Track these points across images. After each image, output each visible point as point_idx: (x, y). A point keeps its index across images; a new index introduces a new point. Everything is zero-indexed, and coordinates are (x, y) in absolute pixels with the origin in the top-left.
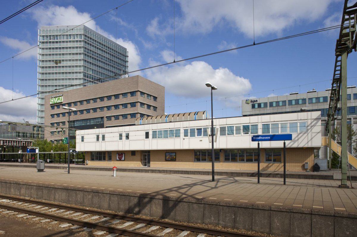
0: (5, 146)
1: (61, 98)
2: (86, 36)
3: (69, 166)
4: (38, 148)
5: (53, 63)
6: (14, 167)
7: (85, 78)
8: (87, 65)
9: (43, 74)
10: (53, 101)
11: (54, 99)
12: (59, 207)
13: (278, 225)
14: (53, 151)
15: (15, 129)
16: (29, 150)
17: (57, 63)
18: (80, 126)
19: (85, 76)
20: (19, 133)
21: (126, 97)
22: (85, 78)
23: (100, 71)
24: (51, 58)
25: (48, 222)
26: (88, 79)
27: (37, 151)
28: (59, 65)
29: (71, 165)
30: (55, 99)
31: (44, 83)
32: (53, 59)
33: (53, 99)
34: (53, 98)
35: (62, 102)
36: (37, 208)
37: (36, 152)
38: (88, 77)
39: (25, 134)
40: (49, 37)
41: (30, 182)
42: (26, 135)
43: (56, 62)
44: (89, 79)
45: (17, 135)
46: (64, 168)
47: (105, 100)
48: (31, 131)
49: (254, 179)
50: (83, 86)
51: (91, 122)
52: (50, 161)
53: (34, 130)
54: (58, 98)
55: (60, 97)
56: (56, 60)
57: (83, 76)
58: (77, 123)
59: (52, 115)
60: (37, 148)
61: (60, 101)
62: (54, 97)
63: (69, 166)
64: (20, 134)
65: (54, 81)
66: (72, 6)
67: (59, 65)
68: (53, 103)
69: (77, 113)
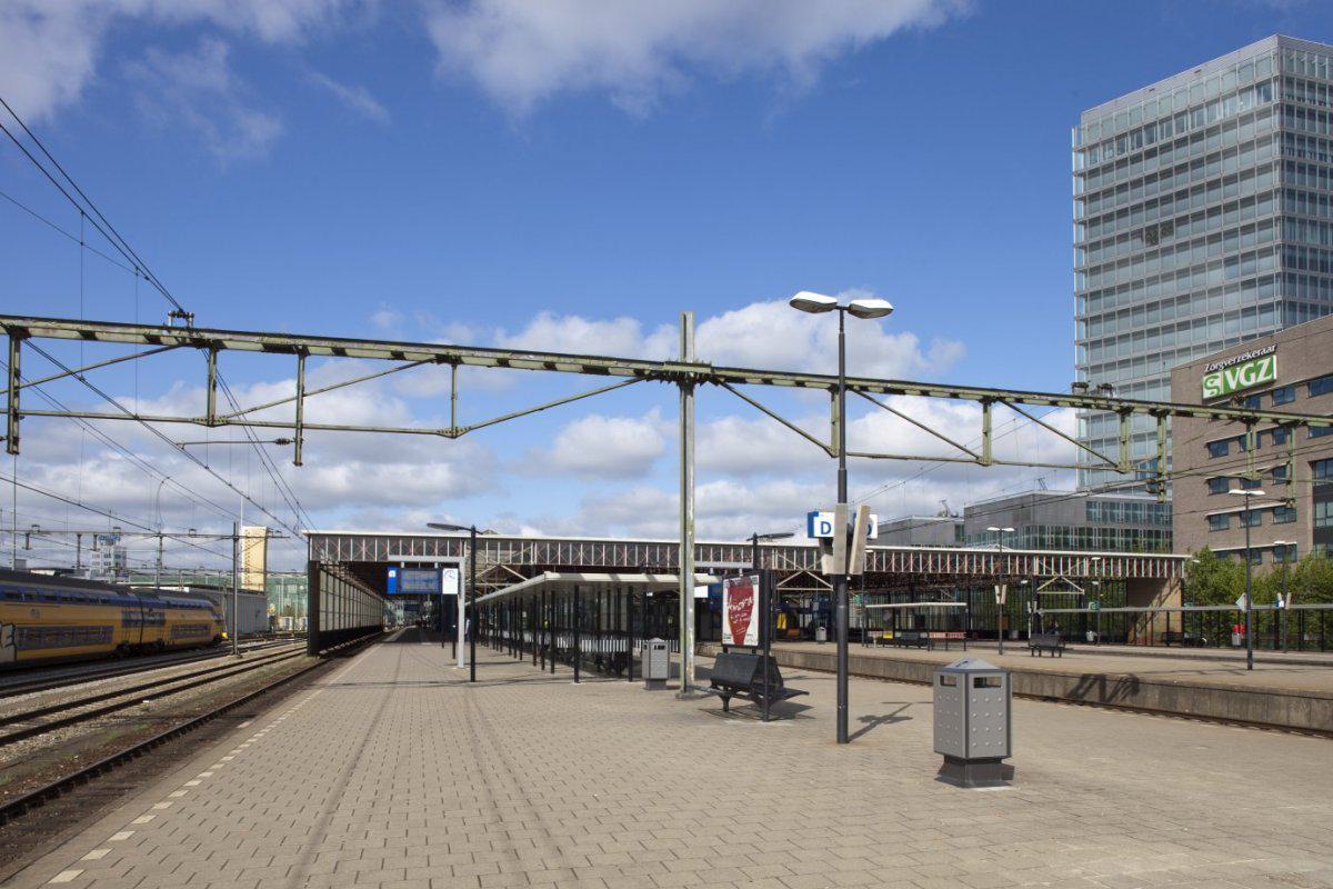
0: (1096, 579)
1: (1271, 363)
2: (1290, 81)
3: (1250, 655)
7: (1292, 271)
10: (1218, 382)
11: (1228, 373)
14: (1292, 602)
15: (1029, 518)
17: (1153, 240)
19: (1288, 261)
22: (1292, 271)
26: (1303, 272)
28: (1165, 242)
30: (1234, 374)
32: (1136, 228)
33: (1218, 374)
34: (1216, 371)
35: (1272, 382)
43: (1151, 235)
44: (1308, 273)
46: (993, 648)
48: (1082, 522)
52: (1095, 637)
53: (1089, 516)
54: (1251, 365)
55: (1266, 362)
56: (1148, 228)
59: (1216, 446)
61: (1262, 378)
62: (1226, 368)
63: (1250, 655)
64: (1070, 537)
65: (1144, 316)
66: (544, 315)
68: (1222, 392)
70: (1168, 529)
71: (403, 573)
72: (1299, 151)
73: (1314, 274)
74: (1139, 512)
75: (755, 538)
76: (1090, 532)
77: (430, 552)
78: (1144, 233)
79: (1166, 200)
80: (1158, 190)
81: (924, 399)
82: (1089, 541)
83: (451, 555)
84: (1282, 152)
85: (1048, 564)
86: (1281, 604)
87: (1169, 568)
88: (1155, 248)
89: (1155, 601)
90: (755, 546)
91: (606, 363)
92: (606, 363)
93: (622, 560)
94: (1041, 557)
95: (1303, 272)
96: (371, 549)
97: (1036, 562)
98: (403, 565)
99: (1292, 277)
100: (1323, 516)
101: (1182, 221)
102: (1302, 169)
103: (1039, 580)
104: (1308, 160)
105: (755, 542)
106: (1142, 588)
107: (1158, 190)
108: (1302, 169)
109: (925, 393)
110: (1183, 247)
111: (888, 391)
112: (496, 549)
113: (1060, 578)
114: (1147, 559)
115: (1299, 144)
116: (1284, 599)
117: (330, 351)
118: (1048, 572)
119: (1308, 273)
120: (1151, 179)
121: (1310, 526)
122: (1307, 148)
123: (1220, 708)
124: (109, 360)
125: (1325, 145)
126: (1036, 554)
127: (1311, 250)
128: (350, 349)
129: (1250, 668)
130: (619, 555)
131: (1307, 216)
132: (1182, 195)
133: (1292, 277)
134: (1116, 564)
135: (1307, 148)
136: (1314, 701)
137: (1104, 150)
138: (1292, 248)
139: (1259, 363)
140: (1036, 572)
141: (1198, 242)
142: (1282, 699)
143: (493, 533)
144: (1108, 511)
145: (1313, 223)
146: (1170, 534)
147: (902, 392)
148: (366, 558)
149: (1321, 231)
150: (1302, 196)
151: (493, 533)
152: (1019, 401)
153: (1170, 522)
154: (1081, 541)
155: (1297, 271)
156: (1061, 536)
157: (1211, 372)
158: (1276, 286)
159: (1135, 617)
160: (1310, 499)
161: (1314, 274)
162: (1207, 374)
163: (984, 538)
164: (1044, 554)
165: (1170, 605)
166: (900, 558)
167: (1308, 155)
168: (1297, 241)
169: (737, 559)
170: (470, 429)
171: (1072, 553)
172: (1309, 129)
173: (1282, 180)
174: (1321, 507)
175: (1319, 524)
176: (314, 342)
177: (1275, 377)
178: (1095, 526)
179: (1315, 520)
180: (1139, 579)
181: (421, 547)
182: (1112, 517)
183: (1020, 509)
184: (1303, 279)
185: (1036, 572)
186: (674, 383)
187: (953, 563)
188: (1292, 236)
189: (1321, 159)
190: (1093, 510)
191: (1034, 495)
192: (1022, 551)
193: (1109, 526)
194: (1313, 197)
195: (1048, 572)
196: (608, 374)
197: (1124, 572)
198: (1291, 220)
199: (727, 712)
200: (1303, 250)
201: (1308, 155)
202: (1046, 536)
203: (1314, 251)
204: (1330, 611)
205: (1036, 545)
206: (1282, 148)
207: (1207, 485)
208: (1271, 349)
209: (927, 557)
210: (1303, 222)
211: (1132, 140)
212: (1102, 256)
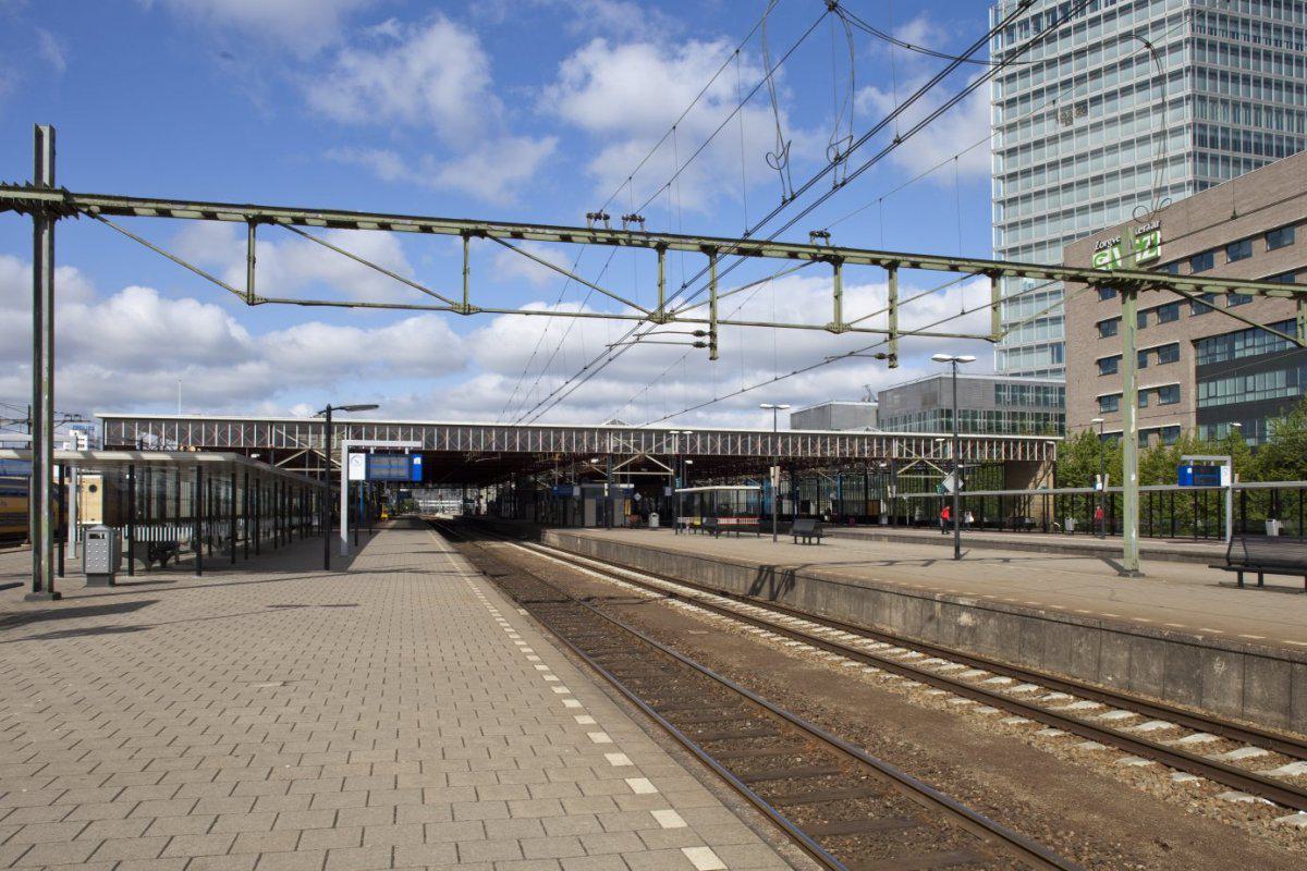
0: (689, 457)
3: (957, 535)
4: (1229, 463)
5: (1053, 121)
6: (848, 538)
7: (1204, 150)
8: (1208, 87)
9: (1012, 176)
12: (895, 641)
13: (1108, 675)
16: (1190, 471)
17: (1068, 121)
18: (1271, 354)
19: (1200, 140)
20: (974, 415)
21: (1289, 242)
22: (1204, 150)
23: (1273, 103)
24: (1043, 105)
25: (855, 667)
26: (1215, 151)
27: (1226, 479)
29: (964, 535)
31: (1020, 212)
33: (1107, 251)
34: (1105, 248)
36: (846, 638)
37: (1219, 484)
38: (1214, 144)
39: (969, 420)
40: (1031, 26)
41: (953, 591)
42: (997, 423)
44: (1219, 152)
45: (942, 423)
47: (1216, 266)
48: (991, 406)
49: (1043, 562)
50: (1195, 189)
51: (1238, 345)
53: (998, 399)
57: (1194, 143)
58: (1249, 342)
60: (1224, 463)
67: (1078, 123)
69: (1177, 310)
70: (1058, 411)
71: (372, 459)
72: (1276, 41)
73: (1247, 156)
74: (1049, 395)
75: (329, 410)
76: (999, 415)
77: (369, 437)
78: (1059, 114)
79: (1081, 79)
80: (1074, 69)
81: (384, 234)
82: (974, 424)
83: (390, 439)
84: (1193, 30)
85: (909, 446)
86: (1099, 486)
87: (973, 448)
88: (1069, 128)
89: (1031, 485)
90: (329, 426)
91: (131, 204)
92: (131, 204)
93: (444, 445)
94: (901, 439)
95: (1215, 151)
96: (453, 439)
97: (895, 444)
98: (372, 452)
99: (1203, 157)
100: (1206, 396)
101: (1096, 100)
102: (1212, 47)
103: (899, 463)
104: (1284, 49)
105: (329, 417)
106: (1018, 471)
107: (1074, 69)
108: (1212, 47)
109: (384, 227)
110: (1096, 127)
111: (332, 224)
112: (308, 433)
113: (922, 462)
114: (1032, 442)
115: (1264, 32)
116: (1103, 481)
117: (199, 214)
118: (909, 454)
119: (1219, 152)
120: (1066, 58)
121: (1193, 407)
122: (1283, 37)
123: (846, 606)
124: (469, 265)
125: (1214, 19)
126: (895, 436)
127: (1222, 128)
128: (177, 211)
129: (958, 557)
130: (734, 444)
131: (1219, 94)
132: (1096, 74)
133: (1203, 157)
134: (999, 446)
135: (1283, 37)
136: (908, 599)
137: (1021, 31)
138: (1203, 127)
139: (1145, 239)
140: (895, 455)
141: (1111, 122)
142: (886, 596)
143: (620, 423)
144: (1018, 394)
145: (1224, 102)
146: (1062, 418)
147: (353, 225)
148: (219, 443)
149: (1234, 112)
150: (1213, 75)
151: (620, 423)
152: (301, 221)
153: (1062, 402)
154: (965, 424)
155: (1208, 150)
156: (994, 421)
157: (1100, 250)
158: (1188, 165)
159: (1016, 499)
160: (1192, 377)
161: (1247, 156)
162: (1097, 251)
163: (910, 419)
164: (970, 438)
165: (1041, 490)
166: (746, 441)
167: (1284, 45)
168: (1208, 121)
169: (406, 438)
170: (481, 311)
171: (979, 436)
172: (1275, 17)
173: (1193, 57)
174: (1203, 386)
175: (1202, 405)
176: (223, 210)
177: (1159, 254)
178: (1004, 410)
179: (1198, 400)
180: (1015, 462)
181: (173, 431)
182: (1022, 400)
183: (925, 392)
184: (1214, 159)
185: (895, 455)
186: (26, 215)
187: (805, 446)
188: (1203, 115)
189: (1255, 41)
190: (1002, 393)
191: (940, 378)
192: (1025, 437)
193: (1019, 409)
194: (1224, 76)
195: (909, 454)
196: (217, 219)
197: (999, 456)
198: (1202, 99)
199: (1240, 585)
200: (1214, 129)
201: (1284, 45)
202: (978, 420)
203: (1225, 130)
204: (1302, 490)
205: (935, 428)
206: (1193, 25)
207: (1098, 367)
208: (1155, 225)
209: (1034, 445)
210: (1214, 101)
211: (1048, 21)
212: (1020, 137)
